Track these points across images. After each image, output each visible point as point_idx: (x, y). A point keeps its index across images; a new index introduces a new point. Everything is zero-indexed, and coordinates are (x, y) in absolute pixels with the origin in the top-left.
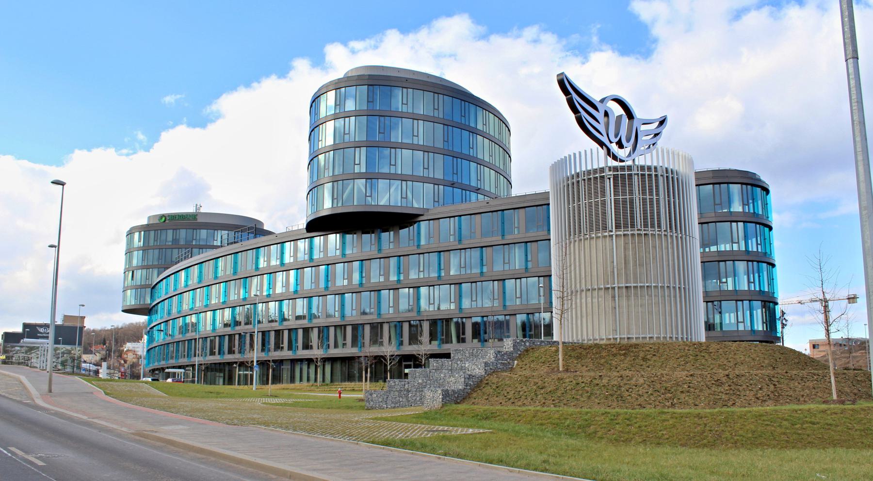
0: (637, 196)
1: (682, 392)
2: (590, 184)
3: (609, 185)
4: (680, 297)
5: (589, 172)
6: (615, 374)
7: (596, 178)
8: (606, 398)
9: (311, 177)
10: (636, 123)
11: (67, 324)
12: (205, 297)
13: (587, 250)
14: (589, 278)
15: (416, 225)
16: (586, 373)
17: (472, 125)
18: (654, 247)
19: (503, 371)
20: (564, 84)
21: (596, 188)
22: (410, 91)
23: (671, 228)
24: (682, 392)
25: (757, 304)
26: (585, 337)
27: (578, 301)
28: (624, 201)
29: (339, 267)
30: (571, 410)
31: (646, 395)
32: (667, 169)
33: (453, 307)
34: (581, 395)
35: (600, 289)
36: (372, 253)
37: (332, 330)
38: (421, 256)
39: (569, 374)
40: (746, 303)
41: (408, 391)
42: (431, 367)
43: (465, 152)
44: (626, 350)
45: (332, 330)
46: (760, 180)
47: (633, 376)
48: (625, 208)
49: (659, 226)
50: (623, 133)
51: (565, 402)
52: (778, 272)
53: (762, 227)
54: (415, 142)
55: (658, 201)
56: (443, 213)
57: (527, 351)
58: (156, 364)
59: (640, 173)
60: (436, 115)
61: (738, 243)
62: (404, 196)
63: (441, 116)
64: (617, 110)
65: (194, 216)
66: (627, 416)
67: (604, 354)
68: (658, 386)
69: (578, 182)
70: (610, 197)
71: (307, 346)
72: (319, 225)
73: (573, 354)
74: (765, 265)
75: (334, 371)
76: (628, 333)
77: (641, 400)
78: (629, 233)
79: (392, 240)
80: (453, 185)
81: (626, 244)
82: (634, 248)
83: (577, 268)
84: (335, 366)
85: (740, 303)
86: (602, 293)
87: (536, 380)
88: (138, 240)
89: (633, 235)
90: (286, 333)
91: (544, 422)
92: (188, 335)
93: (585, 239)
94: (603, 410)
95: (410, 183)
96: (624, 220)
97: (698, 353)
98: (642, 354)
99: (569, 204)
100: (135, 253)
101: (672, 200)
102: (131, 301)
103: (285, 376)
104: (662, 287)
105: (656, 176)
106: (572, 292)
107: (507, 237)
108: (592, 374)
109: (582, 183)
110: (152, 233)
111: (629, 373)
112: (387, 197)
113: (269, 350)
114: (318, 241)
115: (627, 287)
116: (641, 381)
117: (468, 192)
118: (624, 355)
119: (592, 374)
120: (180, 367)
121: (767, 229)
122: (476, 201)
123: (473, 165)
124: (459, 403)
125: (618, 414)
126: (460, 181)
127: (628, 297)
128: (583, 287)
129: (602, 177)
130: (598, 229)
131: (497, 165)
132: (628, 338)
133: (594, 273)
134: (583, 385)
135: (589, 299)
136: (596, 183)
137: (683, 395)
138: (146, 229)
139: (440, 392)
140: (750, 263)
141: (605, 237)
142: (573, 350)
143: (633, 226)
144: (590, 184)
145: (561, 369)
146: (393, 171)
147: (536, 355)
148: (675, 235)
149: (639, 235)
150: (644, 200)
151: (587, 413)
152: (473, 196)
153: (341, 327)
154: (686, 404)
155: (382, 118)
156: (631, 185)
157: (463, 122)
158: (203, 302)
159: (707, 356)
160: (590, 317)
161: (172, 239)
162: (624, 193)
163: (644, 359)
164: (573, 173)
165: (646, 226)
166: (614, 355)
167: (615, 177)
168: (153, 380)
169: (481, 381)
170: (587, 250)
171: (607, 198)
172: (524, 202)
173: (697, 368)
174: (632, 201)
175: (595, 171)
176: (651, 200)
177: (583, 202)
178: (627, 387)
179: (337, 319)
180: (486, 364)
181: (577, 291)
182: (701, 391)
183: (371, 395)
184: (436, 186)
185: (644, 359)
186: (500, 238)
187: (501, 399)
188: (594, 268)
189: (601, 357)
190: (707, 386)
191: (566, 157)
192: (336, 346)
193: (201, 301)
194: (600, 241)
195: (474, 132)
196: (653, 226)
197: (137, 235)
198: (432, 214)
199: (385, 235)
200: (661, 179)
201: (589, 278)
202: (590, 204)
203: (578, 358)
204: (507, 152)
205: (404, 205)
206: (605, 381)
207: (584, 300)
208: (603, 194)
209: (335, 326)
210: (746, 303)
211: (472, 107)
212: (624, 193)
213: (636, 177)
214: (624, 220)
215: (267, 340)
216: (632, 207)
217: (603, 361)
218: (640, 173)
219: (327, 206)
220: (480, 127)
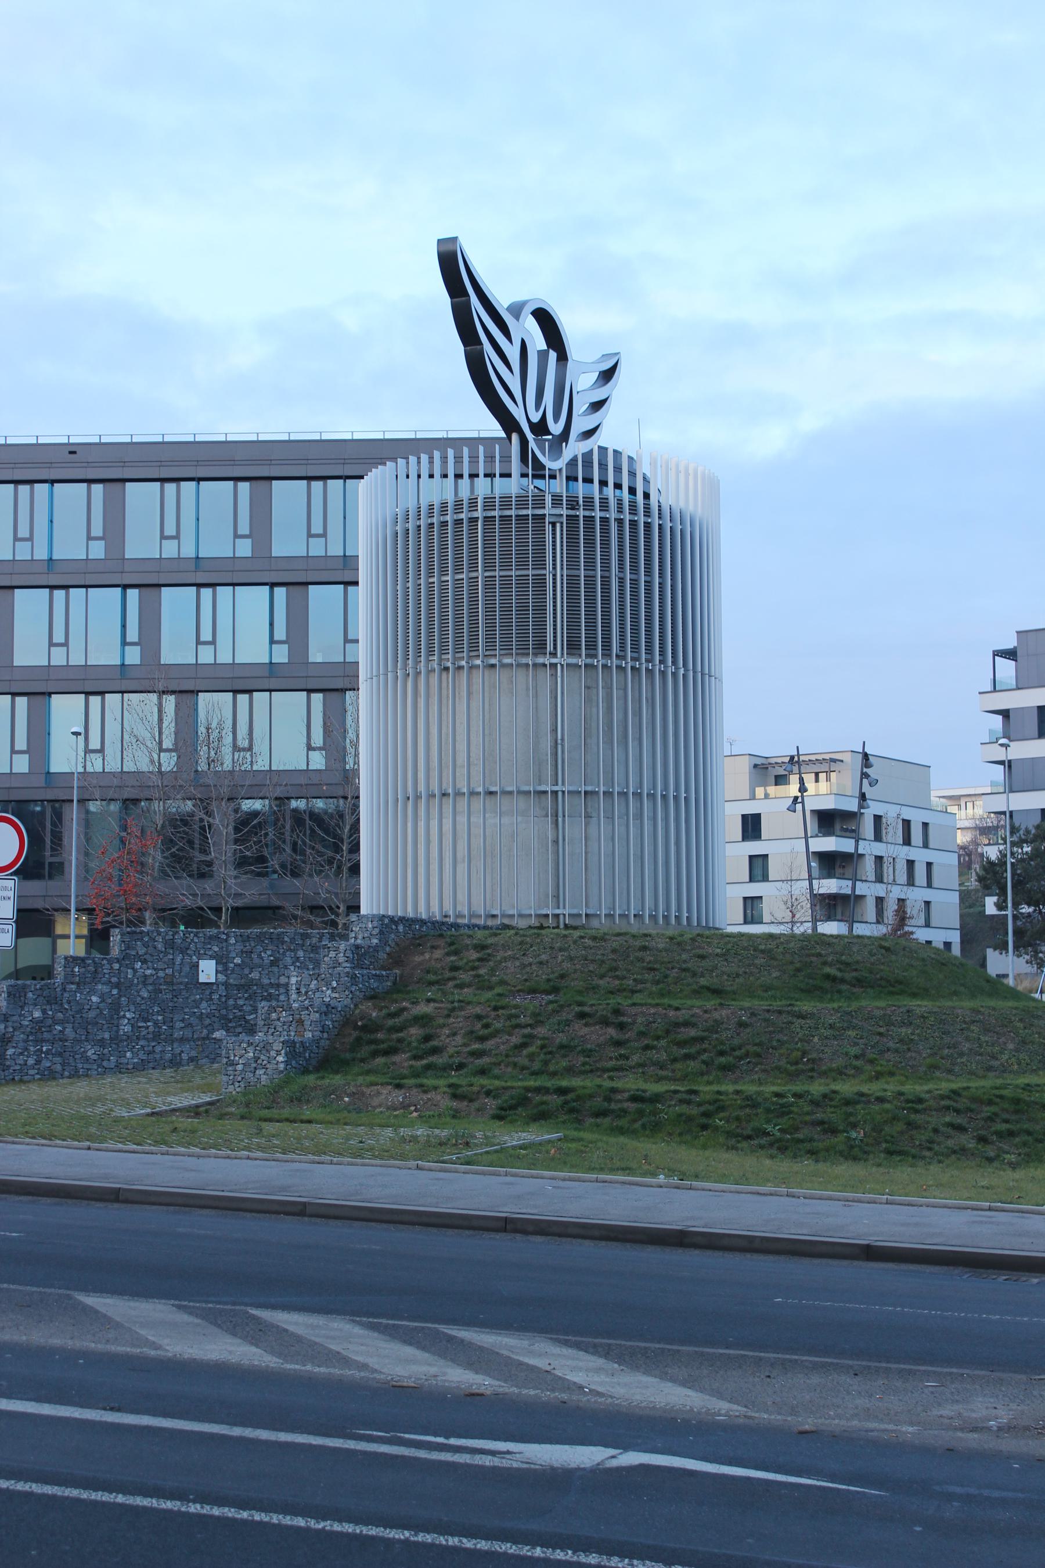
3: (555, 542)
20: (452, 265)
23: (636, 648)
26: (462, 896)
35: (473, 793)
70: (556, 571)
99: (418, 576)
101: (657, 580)
104: (624, 795)
128: (422, 788)
133: (462, 758)
135: (462, 819)
136: (458, 534)
148: (671, 669)
181: (417, 797)
194: (478, 676)
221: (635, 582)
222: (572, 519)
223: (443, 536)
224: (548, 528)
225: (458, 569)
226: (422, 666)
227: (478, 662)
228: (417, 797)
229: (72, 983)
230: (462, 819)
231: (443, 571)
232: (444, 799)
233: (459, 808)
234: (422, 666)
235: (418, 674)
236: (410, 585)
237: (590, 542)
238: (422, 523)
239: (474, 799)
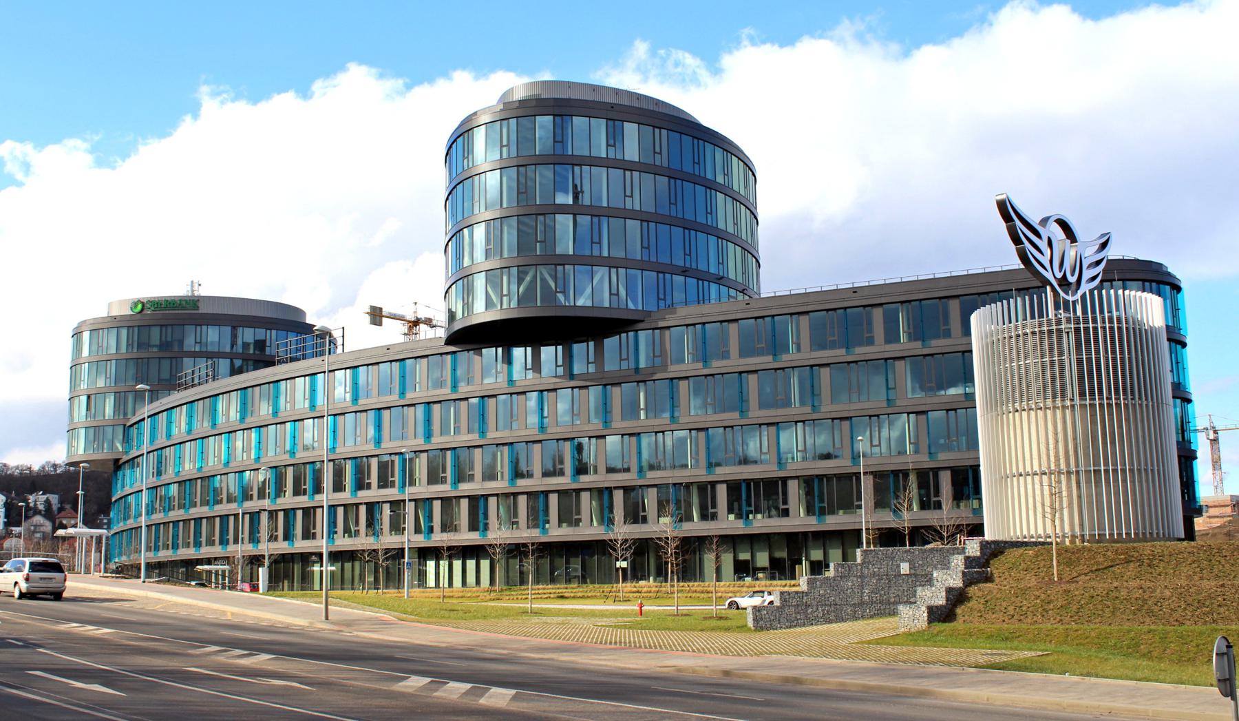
4: (1147, 481)
17: (709, 176)
20: (1006, 210)
21: (1051, 344)
41: (807, 606)
43: (701, 219)
46: (1169, 274)
54: (629, 206)
62: (614, 291)
63: (665, 164)
64: (1058, 233)
71: (397, 527)
88: (111, 343)
92: (171, 513)
94: (1146, 628)
112: (590, 293)
113: (228, 543)
116: (1167, 593)
117: (706, 283)
123: (712, 239)
126: (694, 266)
136: (1050, 338)
137: (1222, 610)
146: (596, 253)
184: (661, 275)
195: (711, 186)
205: (615, 305)
206: (1124, 593)
220: (720, 179)
221: (1114, 359)
222: (1077, 330)
223: (1010, 344)
224: (1064, 335)
231: (1011, 361)
237: (1088, 341)
238: (1000, 337)
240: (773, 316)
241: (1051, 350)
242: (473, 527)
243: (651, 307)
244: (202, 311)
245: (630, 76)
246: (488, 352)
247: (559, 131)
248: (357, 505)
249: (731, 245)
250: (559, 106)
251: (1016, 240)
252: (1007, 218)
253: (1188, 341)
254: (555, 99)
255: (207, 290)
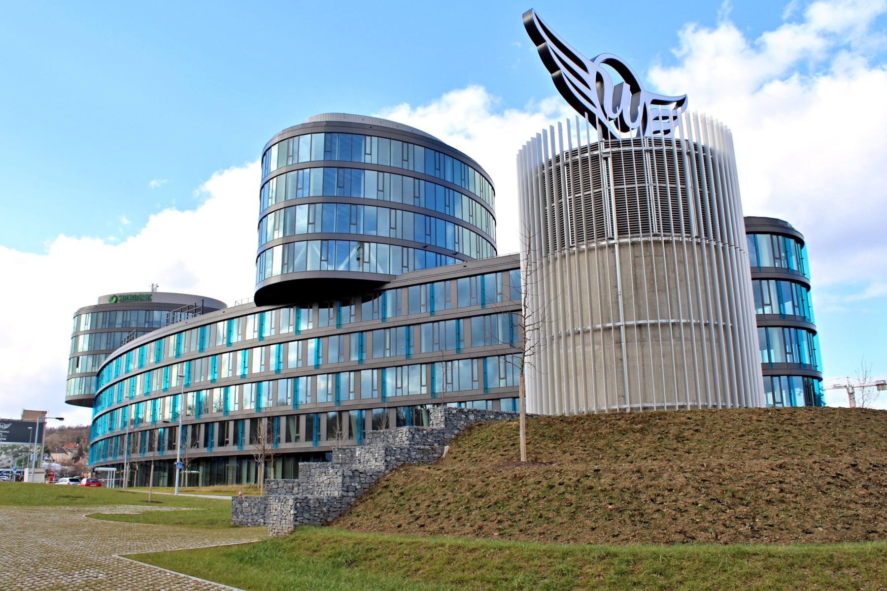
0: (651, 185)
1: (769, 502)
2: (576, 170)
3: (607, 170)
5: (574, 153)
6: (627, 466)
7: (585, 161)
8: (610, 518)
9: (260, 241)
10: (645, 98)
11: (26, 420)
12: (146, 386)
13: (575, 271)
14: (578, 315)
15: (380, 298)
16: (569, 465)
18: (682, 262)
19: (421, 462)
21: (586, 175)
22: (375, 139)
23: (706, 234)
24: (769, 502)
25: (798, 380)
27: (562, 351)
28: (631, 192)
29: (293, 345)
30: (535, 545)
31: (693, 510)
32: (695, 145)
33: (424, 391)
34: (558, 511)
35: (596, 331)
36: (330, 328)
37: (283, 420)
38: (387, 330)
39: (535, 468)
40: (784, 379)
42: (335, 461)
43: (440, 209)
44: (644, 422)
45: (283, 420)
46: (792, 229)
47: (662, 470)
48: (634, 218)
49: (688, 230)
50: (626, 107)
51: (523, 525)
52: (821, 339)
53: (799, 286)
55: (684, 191)
56: (413, 279)
57: (470, 429)
58: (102, 460)
59: (654, 148)
60: (405, 167)
61: (770, 304)
64: (613, 77)
65: (148, 297)
66: (659, 565)
67: (603, 430)
68: (716, 491)
69: (558, 169)
70: (608, 187)
71: (254, 438)
72: (269, 296)
73: (548, 432)
74: (804, 332)
75: (286, 467)
76: (645, 401)
77: (683, 521)
78: (641, 239)
79: (353, 313)
80: (425, 248)
81: (635, 257)
82: (649, 264)
83: (551, 275)
84: (286, 463)
85: (776, 379)
86: (600, 336)
87: (473, 480)
88: (86, 322)
89: (647, 243)
90: (232, 424)
91: (467, 575)
93: (570, 254)
95: (373, 245)
96: (632, 220)
97: (778, 426)
98: (674, 430)
100: (81, 337)
101: (707, 192)
102: (76, 389)
103: (230, 478)
104: (698, 325)
105: (680, 154)
106: (552, 339)
107: (488, 306)
108: (580, 467)
109: (564, 171)
110: (101, 315)
111: (655, 465)
114: (270, 316)
115: (639, 326)
117: (443, 257)
118: (641, 431)
119: (580, 467)
120: (113, 466)
121: (804, 289)
122: (452, 266)
124: (328, 524)
125: (637, 559)
126: (433, 243)
127: (642, 341)
128: (569, 328)
129: (595, 158)
130: (590, 238)
131: (479, 226)
132: (644, 408)
134: (562, 489)
135: (579, 348)
136: (585, 168)
137: (772, 510)
138: (95, 310)
139: (291, 502)
140: (786, 330)
141: (602, 248)
142: (549, 425)
143: (646, 230)
144: (576, 170)
145: (523, 459)
147: (483, 435)
148: (713, 243)
149: (657, 243)
150: (663, 190)
151: (565, 555)
152: (450, 260)
153: (292, 418)
154: (779, 530)
155: (341, 171)
156: (640, 167)
157: (438, 176)
158: (155, 393)
159: (795, 432)
160: (581, 378)
161: (121, 319)
162: (630, 181)
163: (679, 438)
164: (550, 157)
165: (667, 229)
166: (623, 432)
167: (616, 156)
168: (71, 480)
169: (378, 482)
170: (575, 271)
171: (604, 190)
172: (508, 263)
173: (781, 453)
174: (643, 191)
175: (584, 150)
176: (674, 191)
177: (566, 198)
178: (651, 492)
179: (289, 408)
180: (388, 451)
181: (559, 337)
182: (809, 498)
183: (241, 503)
185: (679, 438)
186: (480, 307)
187: (403, 518)
188: (586, 298)
189: (599, 436)
190: (819, 488)
191: (538, 135)
192: (288, 439)
193: (142, 388)
194: (595, 255)
196: (678, 230)
197: (83, 316)
198: (401, 281)
199: (345, 310)
200: (686, 159)
201: (578, 315)
202: (578, 200)
203: (555, 438)
204: (490, 212)
206: (606, 480)
207: (571, 350)
208: (598, 184)
209: (287, 416)
210: (784, 379)
211: (449, 161)
212: (630, 181)
213: (648, 156)
214: (632, 220)
215: (210, 433)
216: (643, 201)
217: (602, 442)
218: (654, 148)
219: (276, 272)
225: (587, 188)
226: (551, 257)
227: (594, 245)
228: (559, 337)
229: (383, 383)
230: (579, 348)
232: (577, 337)
233: (586, 341)
234: (558, 255)
235: (555, 259)
236: (547, 208)
239: (596, 334)
240: (483, 274)
241: (586, 182)
242: (309, 437)
243: (398, 273)
244: (153, 301)
245: (402, 115)
246: (284, 311)
247: (328, 144)
248: (199, 424)
249: (466, 231)
250: (342, 133)
251: (551, 66)
252: (537, 39)
253: (823, 376)
254: (327, 122)
255: (163, 288)
